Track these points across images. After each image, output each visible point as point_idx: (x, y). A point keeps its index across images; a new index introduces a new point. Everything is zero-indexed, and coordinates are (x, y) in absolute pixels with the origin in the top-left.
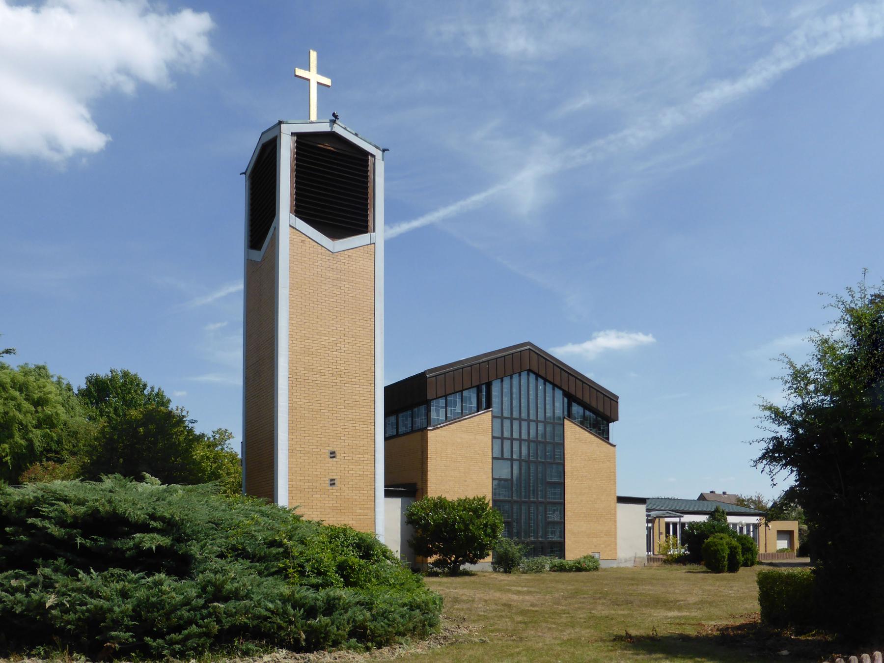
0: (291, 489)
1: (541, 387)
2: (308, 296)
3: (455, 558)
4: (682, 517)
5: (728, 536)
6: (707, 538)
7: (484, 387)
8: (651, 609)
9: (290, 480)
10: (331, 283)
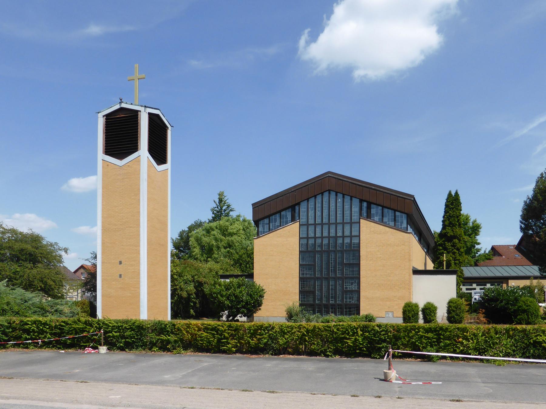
0: (103, 280)
1: (340, 200)
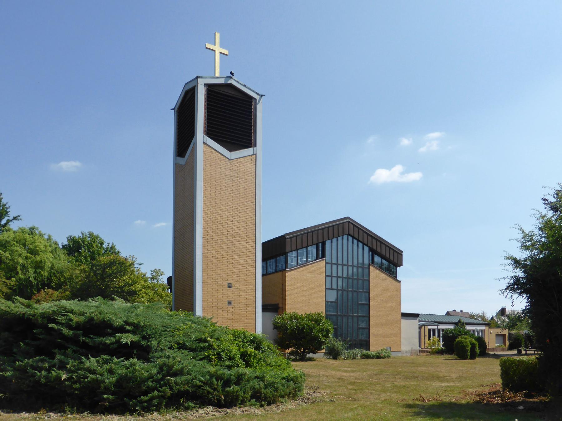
2: (215, 186)
3: (303, 350)
4: (439, 325)
5: (469, 337)
6: (457, 338)
7: (320, 245)
8: (430, 381)
9: (204, 301)
10: (229, 179)
